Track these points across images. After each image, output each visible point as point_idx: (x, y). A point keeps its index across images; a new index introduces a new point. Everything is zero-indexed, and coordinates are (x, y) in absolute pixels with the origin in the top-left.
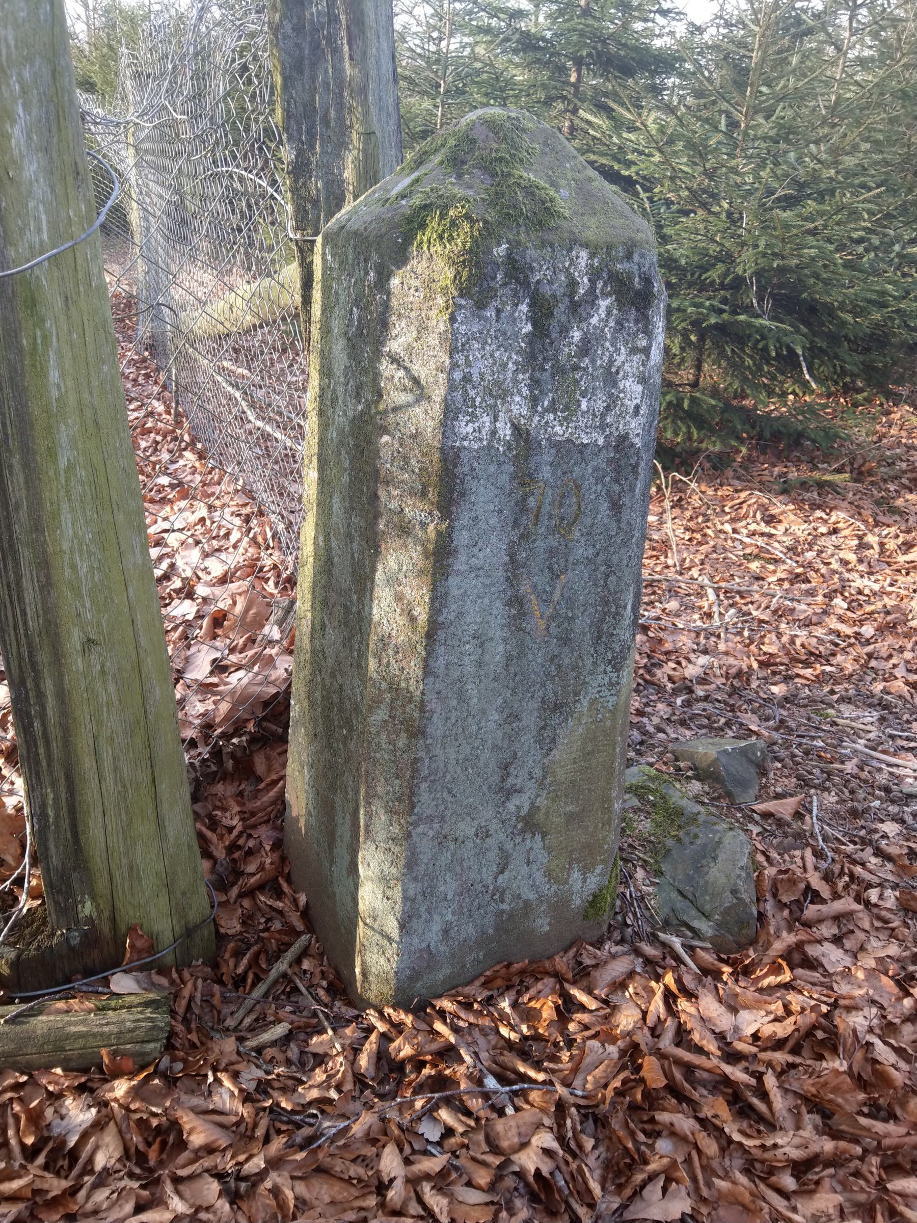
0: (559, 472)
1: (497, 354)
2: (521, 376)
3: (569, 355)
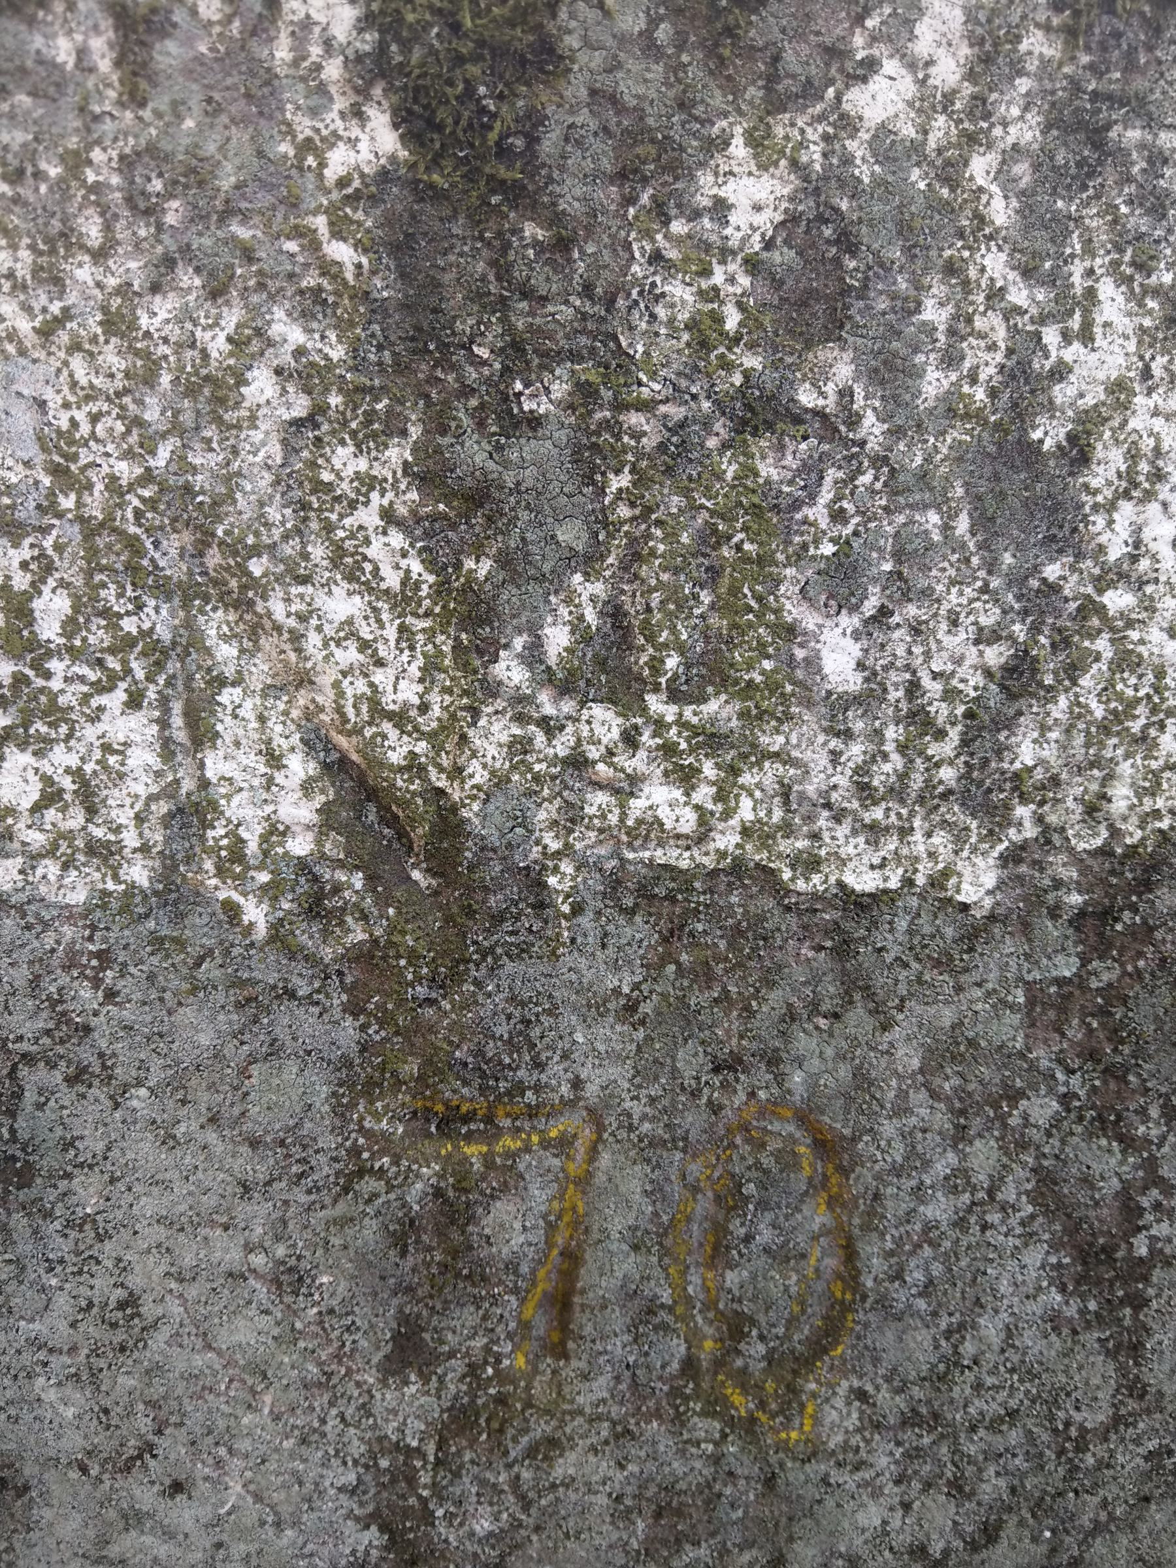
0: (690, 1061)
1: (157, 316)
2: (346, 461)
3: (704, 333)
